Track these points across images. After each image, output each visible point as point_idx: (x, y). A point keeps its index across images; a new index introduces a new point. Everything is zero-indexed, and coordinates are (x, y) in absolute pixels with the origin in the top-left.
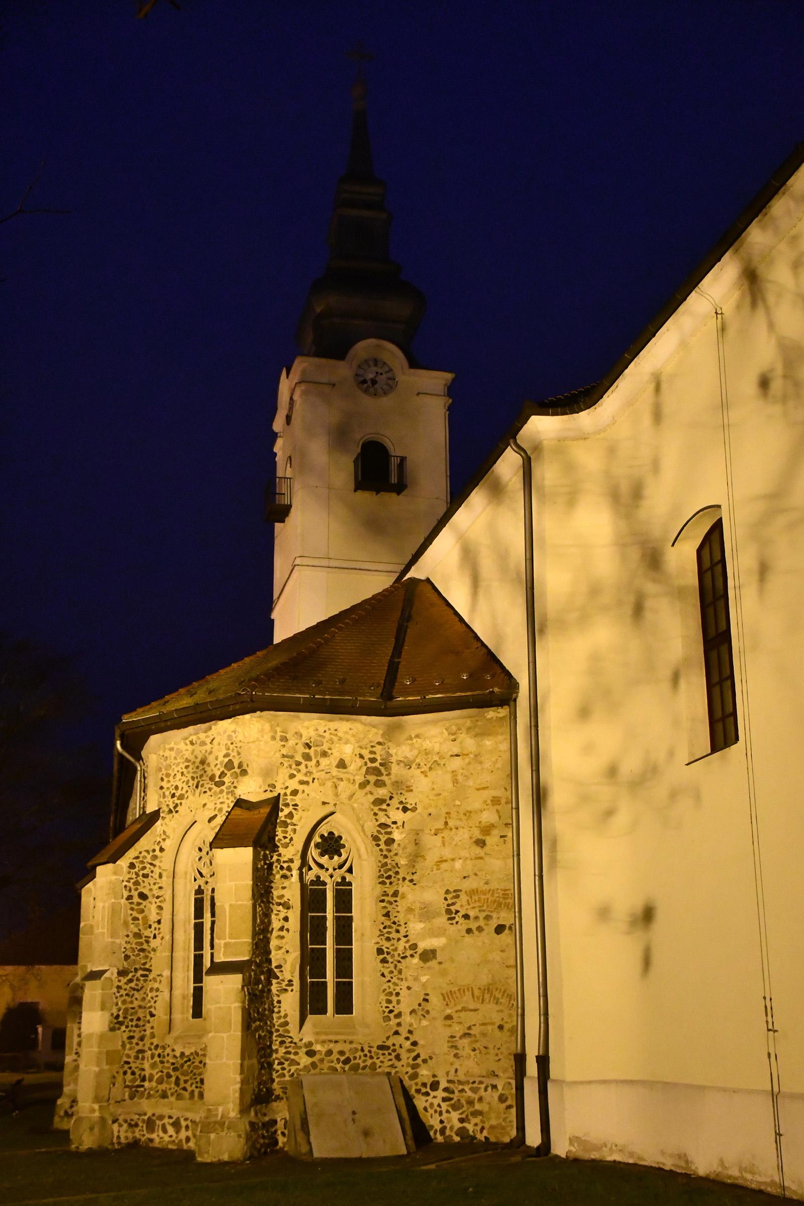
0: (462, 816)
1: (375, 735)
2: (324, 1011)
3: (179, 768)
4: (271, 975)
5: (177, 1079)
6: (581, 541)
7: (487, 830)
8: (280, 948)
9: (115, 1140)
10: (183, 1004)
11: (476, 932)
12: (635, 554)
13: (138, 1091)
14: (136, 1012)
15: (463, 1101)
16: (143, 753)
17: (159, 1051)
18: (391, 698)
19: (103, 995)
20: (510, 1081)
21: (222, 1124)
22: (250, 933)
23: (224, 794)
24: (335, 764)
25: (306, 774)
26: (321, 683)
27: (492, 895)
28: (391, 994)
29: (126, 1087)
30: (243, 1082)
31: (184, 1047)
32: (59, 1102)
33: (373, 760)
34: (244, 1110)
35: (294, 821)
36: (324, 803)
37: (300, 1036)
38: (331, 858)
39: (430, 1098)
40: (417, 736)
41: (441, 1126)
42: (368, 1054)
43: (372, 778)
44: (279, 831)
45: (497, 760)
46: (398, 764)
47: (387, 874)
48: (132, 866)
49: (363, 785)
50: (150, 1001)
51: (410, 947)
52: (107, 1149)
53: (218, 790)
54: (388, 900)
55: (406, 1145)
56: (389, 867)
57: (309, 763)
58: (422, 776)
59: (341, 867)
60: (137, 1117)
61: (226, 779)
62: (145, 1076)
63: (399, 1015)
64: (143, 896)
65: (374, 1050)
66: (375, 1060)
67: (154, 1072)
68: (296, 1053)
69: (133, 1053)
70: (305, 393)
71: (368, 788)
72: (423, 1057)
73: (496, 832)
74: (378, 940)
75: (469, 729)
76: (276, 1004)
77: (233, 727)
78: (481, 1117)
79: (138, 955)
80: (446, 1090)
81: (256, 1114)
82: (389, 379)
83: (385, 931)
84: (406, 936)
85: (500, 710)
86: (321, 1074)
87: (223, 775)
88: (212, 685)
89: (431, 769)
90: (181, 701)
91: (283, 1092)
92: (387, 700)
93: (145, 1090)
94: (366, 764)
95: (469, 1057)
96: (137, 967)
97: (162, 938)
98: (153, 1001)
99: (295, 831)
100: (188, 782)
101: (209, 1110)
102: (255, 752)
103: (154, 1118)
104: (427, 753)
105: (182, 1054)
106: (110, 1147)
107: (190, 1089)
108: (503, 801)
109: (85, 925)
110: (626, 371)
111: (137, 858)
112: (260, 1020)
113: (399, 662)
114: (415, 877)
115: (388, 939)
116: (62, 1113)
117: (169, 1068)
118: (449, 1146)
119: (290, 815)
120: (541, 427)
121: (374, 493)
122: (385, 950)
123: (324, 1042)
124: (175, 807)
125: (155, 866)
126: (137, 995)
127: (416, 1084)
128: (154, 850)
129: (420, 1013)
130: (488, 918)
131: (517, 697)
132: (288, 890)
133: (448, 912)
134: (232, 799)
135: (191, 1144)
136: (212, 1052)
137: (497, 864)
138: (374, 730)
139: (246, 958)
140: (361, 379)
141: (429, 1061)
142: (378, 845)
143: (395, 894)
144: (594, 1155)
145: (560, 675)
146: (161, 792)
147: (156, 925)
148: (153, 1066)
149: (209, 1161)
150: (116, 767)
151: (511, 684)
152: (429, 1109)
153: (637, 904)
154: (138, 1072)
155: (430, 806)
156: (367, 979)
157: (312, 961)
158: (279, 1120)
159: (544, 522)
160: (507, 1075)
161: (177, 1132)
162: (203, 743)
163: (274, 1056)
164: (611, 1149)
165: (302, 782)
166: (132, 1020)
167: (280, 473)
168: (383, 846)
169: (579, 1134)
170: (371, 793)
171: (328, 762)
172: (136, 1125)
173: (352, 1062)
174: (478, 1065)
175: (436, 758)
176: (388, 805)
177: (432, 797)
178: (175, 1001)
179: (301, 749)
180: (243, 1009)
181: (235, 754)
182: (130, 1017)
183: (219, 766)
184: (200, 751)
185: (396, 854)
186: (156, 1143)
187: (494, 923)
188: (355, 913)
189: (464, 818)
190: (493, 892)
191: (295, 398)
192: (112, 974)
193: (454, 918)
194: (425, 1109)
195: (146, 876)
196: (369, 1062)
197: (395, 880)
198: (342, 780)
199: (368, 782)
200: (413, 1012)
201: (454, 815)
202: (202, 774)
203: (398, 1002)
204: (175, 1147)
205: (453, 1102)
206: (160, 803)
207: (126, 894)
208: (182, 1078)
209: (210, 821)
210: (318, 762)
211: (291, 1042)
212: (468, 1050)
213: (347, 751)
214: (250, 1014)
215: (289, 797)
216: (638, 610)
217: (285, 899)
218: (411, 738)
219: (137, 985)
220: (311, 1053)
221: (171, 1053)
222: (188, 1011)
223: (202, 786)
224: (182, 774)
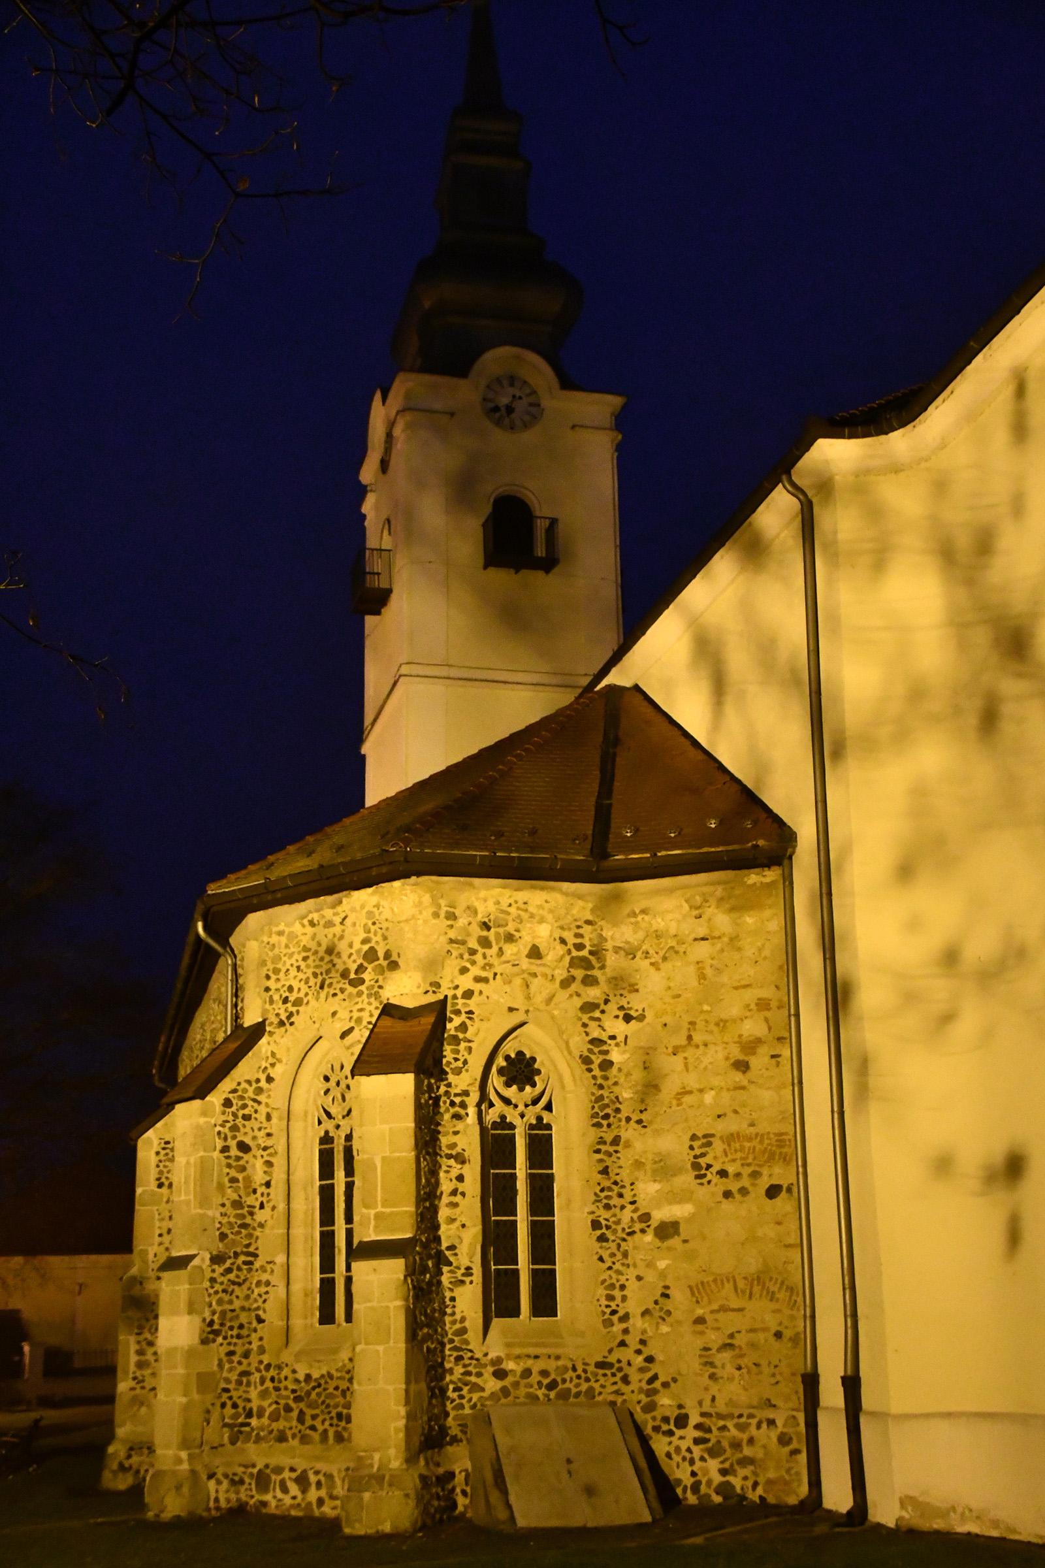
0: (712, 1027)
1: (582, 909)
2: (515, 1312)
3: (293, 961)
4: (441, 1260)
5: (301, 1413)
6: (893, 621)
7: (751, 1046)
8: (454, 1220)
9: (212, 1504)
10: (305, 1303)
11: (737, 1196)
12: (982, 637)
13: (241, 1432)
14: (237, 1317)
15: (725, 1444)
16: (232, 940)
17: (272, 1372)
18: (605, 855)
19: (191, 1293)
20: (794, 1413)
21: (379, 1479)
22: (414, 1200)
23: (365, 996)
24: (526, 952)
25: (484, 968)
26: (502, 835)
27: (761, 1142)
28: (612, 1286)
29: (225, 1425)
30: (410, 1417)
31: (311, 1366)
32: (111, 1449)
33: (579, 947)
34: (411, 1460)
35: (468, 1035)
36: (511, 1010)
37: (484, 1349)
38: (521, 1089)
39: (674, 1439)
40: (643, 912)
41: (692, 1480)
42: (583, 1375)
43: (579, 973)
44: (448, 1050)
45: (763, 945)
46: (616, 953)
47: (603, 1113)
48: (227, 1103)
49: (566, 983)
50: (256, 1301)
51: (639, 1217)
52: (201, 1518)
53: (354, 991)
54: (606, 1149)
55: (650, 1507)
56: (606, 1101)
57: (488, 952)
58: (652, 970)
59: (535, 1102)
60: (242, 1469)
61: (366, 976)
62: (251, 1409)
63: (625, 1318)
64: (244, 1147)
65: (591, 1368)
66: (592, 1383)
67: (265, 1404)
68: (479, 1375)
69: (234, 1377)
70: (409, 426)
71: (574, 987)
72: (662, 1379)
73: (764, 1051)
74: (593, 1208)
75: (721, 900)
76: (448, 1302)
77: (374, 900)
78: (752, 1468)
79: (239, 1233)
80: (698, 1427)
81: (427, 1463)
82: (531, 405)
83: (603, 1195)
85: (767, 872)
86: (515, 1404)
87: (361, 969)
88: (339, 839)
89: (665, 959)
90: (292, 863)
91: (462, 1431)
92: (600, 860)
93: (253, 1429)
94: (569, 952)
95: (731, 1379)
96: (238, 1250)
97: (274, 1208)
98: (261, 1301)
99: (470, 1050)
100: (307, 982)
101: (360, 1459)
102: (410, 935)
103: (268, 1471)
104: (658, 935)
105: (308, 1377)
106: (205, 1514)
107: (320, 1428)
108: (774, 1004)
109: (144, 1192)
110: (969, 368)
111: (234, 1091)
112: (428, 1326)
113: (610, 805)
114: (643, 1117)
115: (607, 1207)
116: (115, 1466)
117: (288, 1397)
118: (704, 1510)
119: (463, 1027)
120: (833, 454)
121: (512, 571)
122: (604, 1223)
123: (518, 1357)
124: (289, 1018)
125: (259, 1103)
126: (238, 1291)
127: (654, 1419)
128: (258, 1081)
129: (657, 1314)
130: (755, 1175)
131: (794, 852)
132: (463, 1137)
133: (696, 1166)
134: (376, 1004)
135: (327, 1510)
136: (361, 1372)
137: (768, 1098)
138: (581, 903)
139: (409, 1235)
140: (491, 405)
141: (672, 1385)
142: (590, 1070)
143: (616, 1141)
144: (938, 1525)
145: (867, 817)
146: (267, 995)
147: (263, 1189)
148: (264, 1394)
149: (362, 1532)
150: (186, 961)
151: (785, 836)
152: (674, 1456)
153: (997, 1152)
154: (241, 1403)
155: (665, 1012)
156: (578, 1264)
157: (498, 1240)
158: (457, 1472)
159: (842, 594)
160: (791, 1405)
161: (304, 1491)
162: (329, 924)
163: (448, 1378)
164: (963, 1514)
165: (478, 979)
166: (231, 1328)
167: (372, 542)
168: (597, 1072)
169: (911, 1493)
170: (578, 995)
171: (515, 950)
172: (242, 1482)
173: (560, 1387)
174: (746, 1390)
175: (672, 943)
176: (603, 1012)
177: (668, 1000)
178: (293, 1300)
179: (477, 931)
180: (407, 1309)
181: (379, 938)
182: (228, 1324)
183: (354, 957)
184: (325, 936)
185: (616, 1084)
186: (272, 1508)
187: (765, 1183)
188: (557, 1169)
189: (716, 1029)
190: (761, 1137)
191: (398, 431)
192: (203, 1260)
193: (705, 1176)
194: (668, 1455)
195: (247, 1118)
196: (584, 1387)
197: (615, 1120)
198: (535, 975)
199: (574, 978)
200: (646, 1313)
201: (700, 1025)
202: (330, 968)
203: (624, 1298)
204: (300, 1514)
205: (710, 1445)
206: (265, 1011)
207: (219, 1144)
208: (309, 1412)
209: (344, 1035)
210: (500, 949)
211: (471, 1358)
212: (730, 1369)
213: (543, 933)
214: (415, 1317)
215: (460, 1001)
216: (989, 719)
217: (458, 1149)
218: (634, 915)
219: (238, 1277)
220: (500, 1374)
221: (291, 1376)
222: (313, 1314)
223: (330, 985)
224: (298, 968)
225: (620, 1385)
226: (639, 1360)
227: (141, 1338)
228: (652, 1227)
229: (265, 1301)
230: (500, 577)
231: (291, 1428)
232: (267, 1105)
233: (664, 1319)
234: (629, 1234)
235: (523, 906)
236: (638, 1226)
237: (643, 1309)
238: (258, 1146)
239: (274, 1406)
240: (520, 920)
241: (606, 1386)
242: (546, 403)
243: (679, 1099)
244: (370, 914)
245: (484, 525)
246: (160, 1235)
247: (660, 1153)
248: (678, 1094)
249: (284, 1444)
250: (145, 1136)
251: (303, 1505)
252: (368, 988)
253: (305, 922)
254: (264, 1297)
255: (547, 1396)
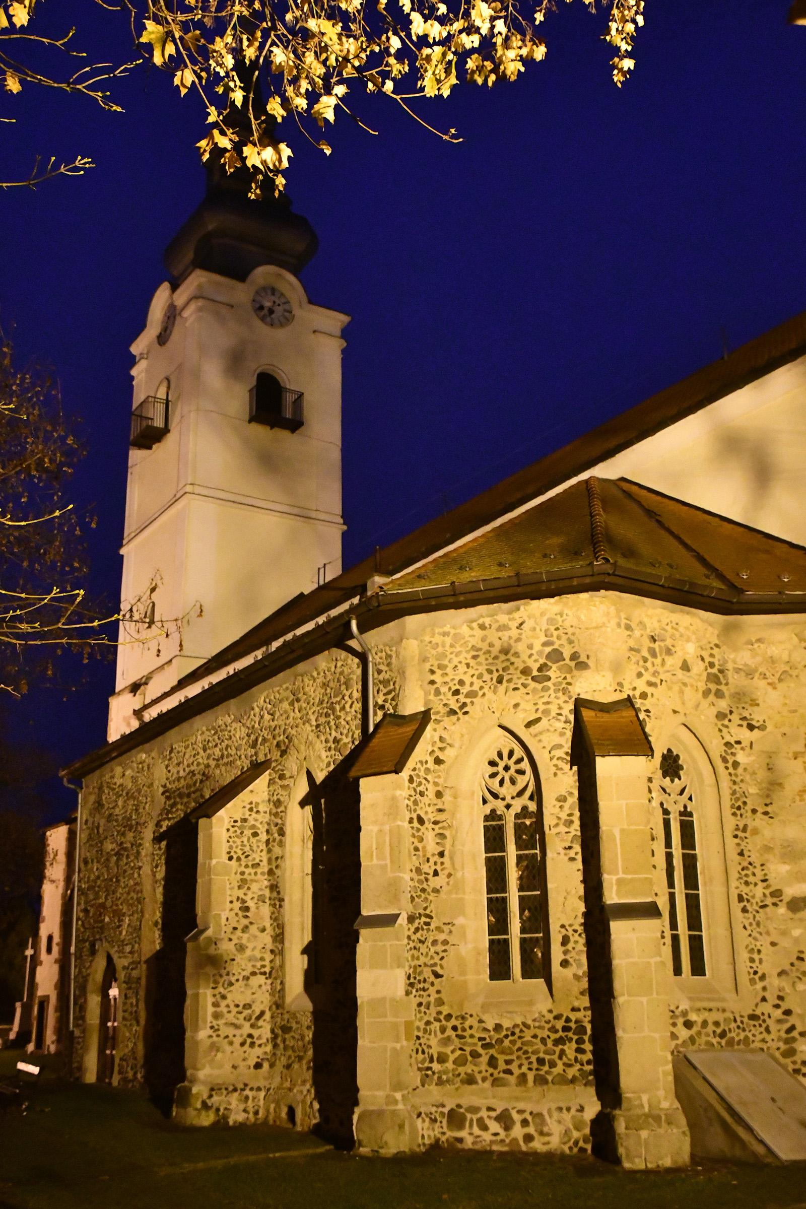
17: (453, 1022)
23: (551, 692)
40: (759, 640)
48: (411, 780)
49: (706, 693)
58: (770, 689)
63: (763, 977)
65: (746, 1020)
67: (448, 1050)
82: (286, 311)
83: (743, 873)
84: (764, 881)
89: (780, 680)
93: (434, 1073)
104: (773, 660)
105: (498, 1028)
107: (517, 1072)
114: (769, 809)
115: (747, 883)
116: (199, 1105)
117: (475, 1045)
121: (269, 428)
122: (745, 896)
124: (461, 708)
127: (794, 1063)
129: (794, 974)
147: (436, 858)
148: (447, 1041)
154: (426, 1050)
161: (507, 1128)
165: (651, 684)
179: (647, 643)
181: (564, 641)
183: (534, 657)
186: (469, 1142)
200: (781, 973)
203: (761, 961)
204: (505, 1149)
208: (501, 1058)
220: (688, 1025)
225: (765, 1035)
226: (778, 1013)
227: (216, 992)
228: (785, 901)
229: (442, 958)
230: (260, 431)
231: (480, 1072)
232: (436, 784)
233: (800, 979)
234: (762, 907)
235: (675, 626)
236: (769, 901)
237: (779, 970)
238: (429, 820)
239: (459, 1052)
240: (672, 637)
241: (755, 1033)
242: (297, 312)
243: (801, 796)
244: (551, 621)
245: (250, 391)
246: (231, 902)
247: (787, 840)
248: (800, 791)
249: (474, 1086)
250: (218, 814)
251: (507, 1141)
252: (554, 685)
253: (475, 625)
254: (442, 954)
255: (719, 1043)
